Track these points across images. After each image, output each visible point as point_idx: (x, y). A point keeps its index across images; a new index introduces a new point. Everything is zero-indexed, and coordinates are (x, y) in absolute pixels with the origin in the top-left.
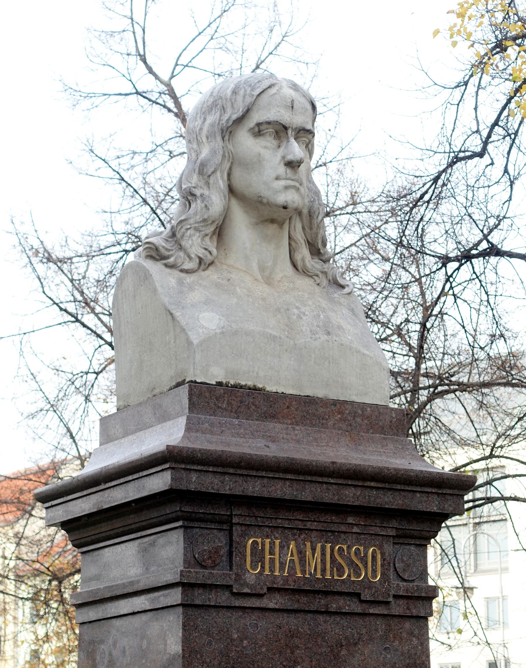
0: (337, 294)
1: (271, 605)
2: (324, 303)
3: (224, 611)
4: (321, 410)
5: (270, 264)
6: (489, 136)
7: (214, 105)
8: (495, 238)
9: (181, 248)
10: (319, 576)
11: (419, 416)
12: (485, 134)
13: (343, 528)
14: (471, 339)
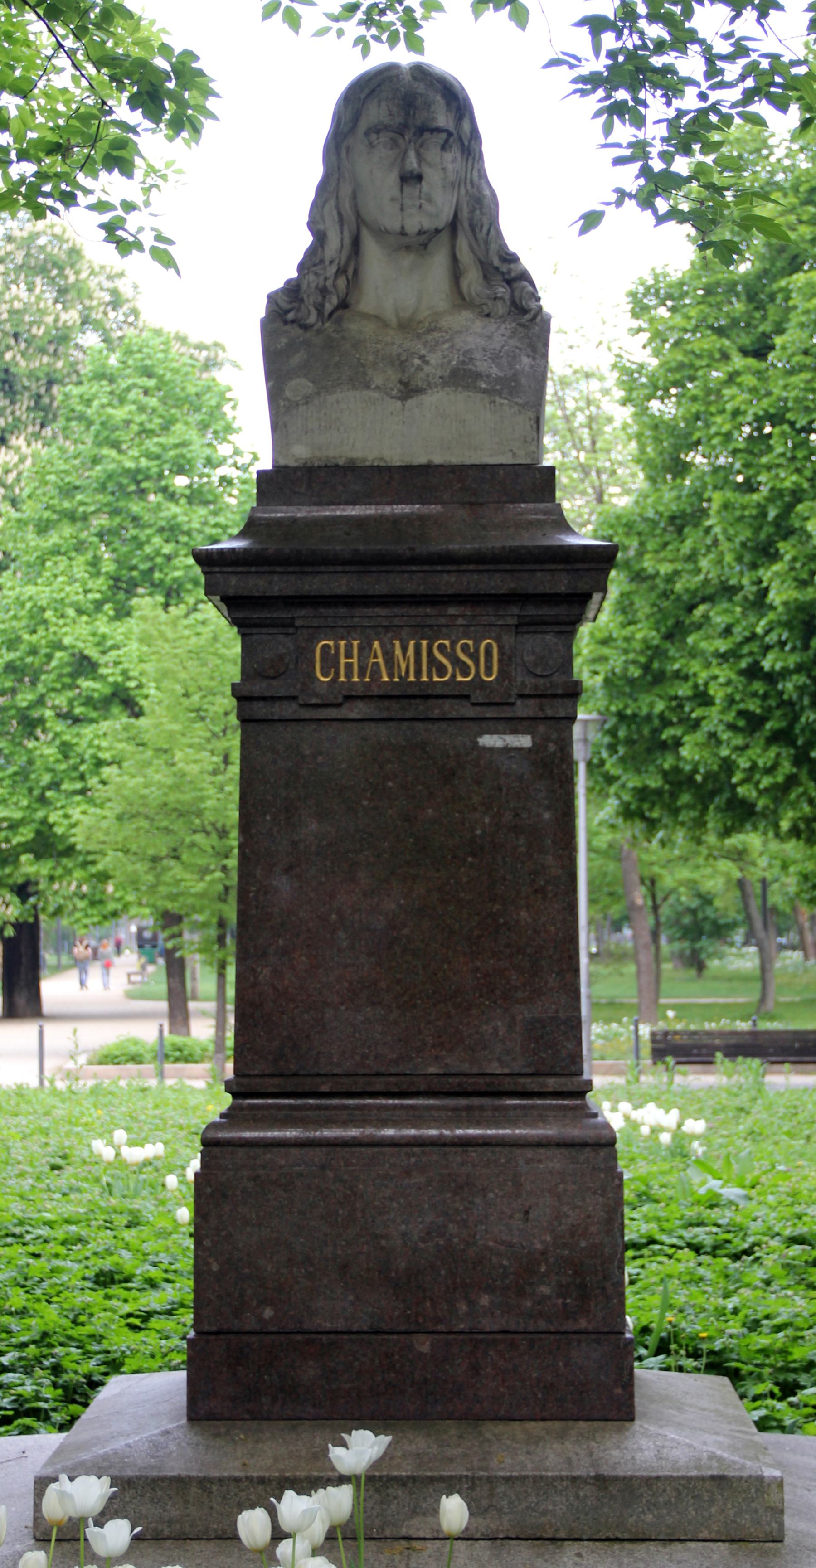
1: (352, 715)
13: (443, 621)
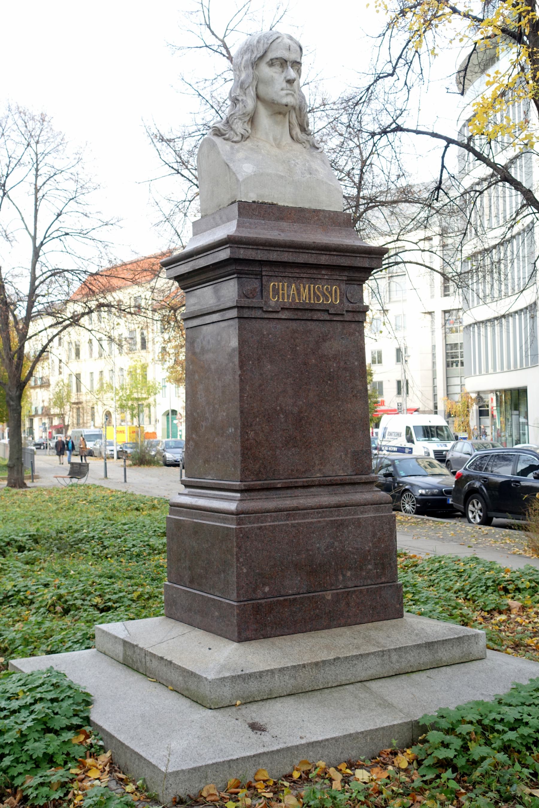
0: (315, 153)
1: (283, 317)
2: (308, 157)
3: (259, 320)
4: (307, 215)
5: (279, 137)
6: (396, 64)
7: (248, 49)
8: (399, 121)
9: (232, 129)
10: (307, 301)
11: (359, 220)
12: (394, 63)
13: (319, 276)
14: (387, 178)
